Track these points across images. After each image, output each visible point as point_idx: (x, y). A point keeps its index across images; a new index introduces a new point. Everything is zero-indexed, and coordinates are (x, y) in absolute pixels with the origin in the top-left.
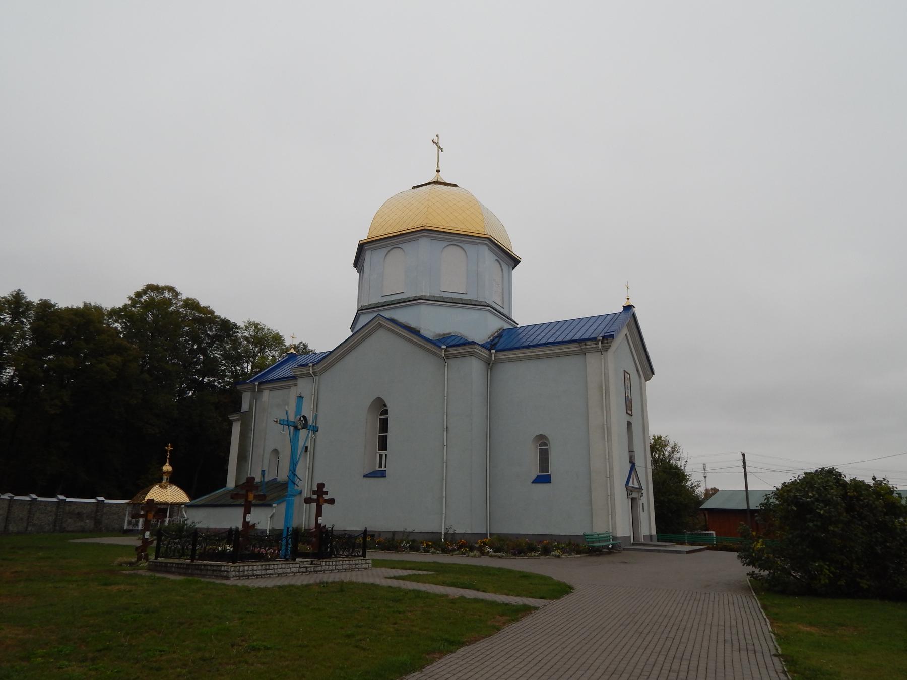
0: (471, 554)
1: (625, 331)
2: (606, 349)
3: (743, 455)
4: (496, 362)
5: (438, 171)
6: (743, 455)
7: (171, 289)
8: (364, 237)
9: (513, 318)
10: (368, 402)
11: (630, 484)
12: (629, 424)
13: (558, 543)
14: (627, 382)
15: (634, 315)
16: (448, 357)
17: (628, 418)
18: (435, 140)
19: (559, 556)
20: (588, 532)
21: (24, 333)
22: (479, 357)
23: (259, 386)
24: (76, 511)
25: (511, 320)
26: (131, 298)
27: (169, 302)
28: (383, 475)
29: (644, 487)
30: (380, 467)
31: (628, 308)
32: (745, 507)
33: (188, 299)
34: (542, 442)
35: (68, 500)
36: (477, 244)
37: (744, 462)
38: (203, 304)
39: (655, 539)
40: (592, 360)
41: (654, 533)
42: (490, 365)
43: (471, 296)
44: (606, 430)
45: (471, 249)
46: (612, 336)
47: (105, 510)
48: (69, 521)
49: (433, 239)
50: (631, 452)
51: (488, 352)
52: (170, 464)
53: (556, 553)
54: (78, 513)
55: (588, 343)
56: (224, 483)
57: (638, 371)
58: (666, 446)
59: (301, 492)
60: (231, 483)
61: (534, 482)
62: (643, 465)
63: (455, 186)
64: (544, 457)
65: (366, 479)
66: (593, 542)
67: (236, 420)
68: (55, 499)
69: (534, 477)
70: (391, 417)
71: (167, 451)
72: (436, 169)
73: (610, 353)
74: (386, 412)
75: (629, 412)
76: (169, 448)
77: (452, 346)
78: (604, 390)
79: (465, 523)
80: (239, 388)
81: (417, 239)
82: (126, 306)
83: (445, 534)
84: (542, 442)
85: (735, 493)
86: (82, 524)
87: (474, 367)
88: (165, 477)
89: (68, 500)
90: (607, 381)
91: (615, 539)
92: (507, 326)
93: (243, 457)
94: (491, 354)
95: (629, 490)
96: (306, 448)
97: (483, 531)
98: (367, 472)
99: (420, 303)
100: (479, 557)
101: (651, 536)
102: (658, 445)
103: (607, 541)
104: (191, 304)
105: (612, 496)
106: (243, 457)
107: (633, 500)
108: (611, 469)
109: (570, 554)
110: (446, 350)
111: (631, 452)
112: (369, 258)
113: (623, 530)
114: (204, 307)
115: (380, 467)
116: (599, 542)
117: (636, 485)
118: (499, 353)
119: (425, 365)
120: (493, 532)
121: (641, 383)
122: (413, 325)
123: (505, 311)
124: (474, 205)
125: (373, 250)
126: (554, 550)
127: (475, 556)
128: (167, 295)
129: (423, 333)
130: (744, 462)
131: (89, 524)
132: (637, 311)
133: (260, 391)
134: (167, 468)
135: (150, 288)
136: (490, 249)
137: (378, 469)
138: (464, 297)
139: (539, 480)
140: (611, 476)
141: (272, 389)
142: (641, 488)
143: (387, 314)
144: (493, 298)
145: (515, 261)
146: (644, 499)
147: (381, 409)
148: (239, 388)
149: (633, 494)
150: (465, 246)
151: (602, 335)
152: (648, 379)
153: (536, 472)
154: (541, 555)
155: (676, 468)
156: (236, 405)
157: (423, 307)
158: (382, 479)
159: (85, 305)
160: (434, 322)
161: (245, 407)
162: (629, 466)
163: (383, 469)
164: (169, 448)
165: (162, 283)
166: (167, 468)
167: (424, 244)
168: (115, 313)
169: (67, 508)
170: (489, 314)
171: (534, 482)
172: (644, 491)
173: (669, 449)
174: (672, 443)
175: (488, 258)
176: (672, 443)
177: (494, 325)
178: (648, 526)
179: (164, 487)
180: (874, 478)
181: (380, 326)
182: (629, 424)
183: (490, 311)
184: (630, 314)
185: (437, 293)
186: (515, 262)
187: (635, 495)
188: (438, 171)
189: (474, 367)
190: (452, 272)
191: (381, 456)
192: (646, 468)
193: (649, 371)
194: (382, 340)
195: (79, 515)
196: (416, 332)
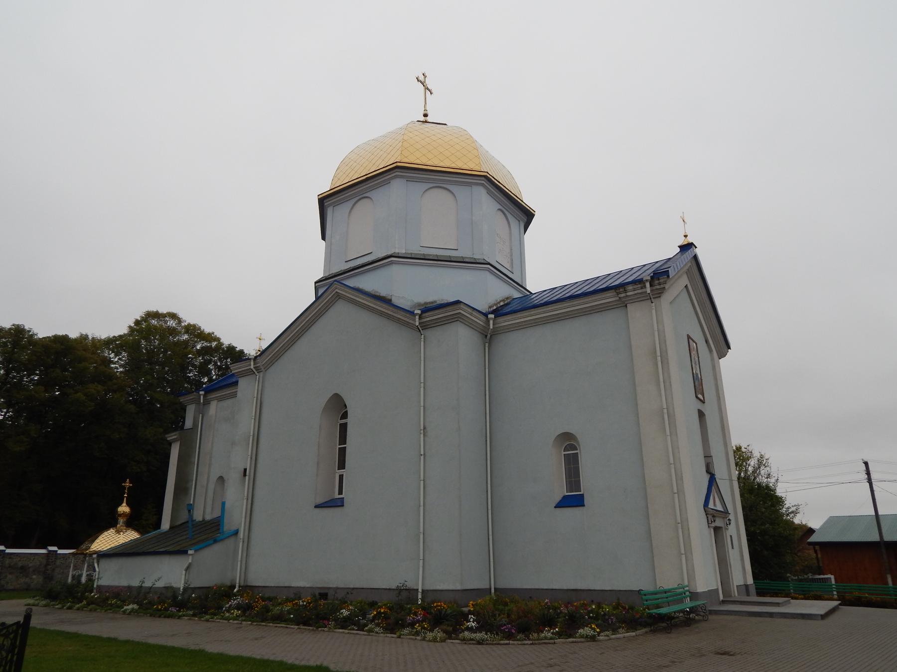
0: (430, 635)
1: (684, 281)
2: (658, 293)
3: (866, 464)
4: (496, 333)
6: (866, 464)
7: (173, 316)
8: (325, 187)
11: (711, 505)
12: (701, 414)
13: (599, 606)
14: (694, 353)
15: (695, 257)
16: (425, 326)
17: (699, 406)
18: (422, 78)
19: (593, 638)
20: (645, 585)
22: (470, 325)
23: (205, 396)
24: (20, 564)
26: (130, 327)
27: (173, 331)
28: (338, 503)
29: (730, 510)
31: (686, 247)
32: (875, 538)
33: (189, 325)
34: (568, 443)
35: (8, 551)
36: (470, 184)
37: (868, 473)
38: (207, 329)
39: (753, 590)
40: (637, 313)
41: (750, 580)
42: (488, 337)
44: (666, 417)
45: (462, 192)
46: (667, 273)
47: (58, 562)
48: (10, 576)
50: (708, 457)
51: (483, 318)
52: (128, 504)
53: (586, 631)
54: (22, 568)
55: (630, 287)
56: (158, 525)
57: (707, 341)
58: (748, 458)
59: (236, 533)
60: (165, 525)
61: (558, 506)
62: (726, 476)
64: (572, 466)
65: (318, 510)
66: (658, 607)
67: (175, 440)
68: (43, 551)
69: (558, 498)
70: (350, 420)
71: (124, 488)
72: (422, 112)
73: (667, 297)
74: (345, 415)
75: (700, 396)
76: (127, 484)
77: (435, 315)
78: (659, 356)
79: (447, 571)
80: (182, 399)
81: (388, 182)
82: (125, 335)
83: (423, 591)
84: (568, 443)
85: (852, 520)
86: (27, 580)
87: (461, 340)
88: (121, 521)
89: (8, 551)
90: (663, 342)
91: (694, 596)
92: (517, 295)
93: (182, 489)
94: (488, 320)
95: (711, 515)
98: (320, 501)
99: (392, 263)
100: (443, 641)
101: (747, 586)
102: (741, 457)
103: (681, 601)
104: (194, 331)
105: (684, 524)
106: (182, 489)
107: (716, 529)
108: (680, 479)
109: (615, 631)
110: (420, 317)
111: (708, 457)
113: (705, 580)
114: (209, 334)
115: (340, 492)
119: (395, 340)
121: (712, 359)
122: (383, 293)
125: (335, 205)
126: (583, 626)
127: (434, 640)
128: (172, 323)
129: (395, 301)
130: (868, 473)
131: (37, 579)
132: (699, 252)
133: (207, 403)
134: (124, 508)
135: (150, 315)
136: (489, 193)
137: (337, 496)
138: (453, 254)
140: (680, 492)
141: (220, 399)
142: (726, 512)
144: (499, 258)
145: (527, 216)
146: (731, 530)
147: (338, 407)
148: (182, 399)
149: (715, 519)
152: (722, 355)
153: (561, 490)
154: (560, 635)
155: (767, 487)
156: (177, 423)
157: (395, 268)
160: (410, 287)
161: (189, 424)
162: (706, 478)
164: (127, 484)
165: (163, 310)
166: (124, 508)
168: (109, 343)
169: (7, 561)
171: (558, 506)
172: (731, 517)
173: (753, 462)
174: (756, 454)
175: (486, 205)
176: (756, 454)
178: (742, 572)
179: (118, 532)
181: (338, 297)
182: (701, 414)
184: (689, 254)
185: (415, 250)
187: (719, 523)
189: (461, 340)
190: (437, 221)
191: (341, 477)
192: (731, 480)
193: (723, 344)
194: (342, 314)
195: (24, 569)
196: (386, 301)
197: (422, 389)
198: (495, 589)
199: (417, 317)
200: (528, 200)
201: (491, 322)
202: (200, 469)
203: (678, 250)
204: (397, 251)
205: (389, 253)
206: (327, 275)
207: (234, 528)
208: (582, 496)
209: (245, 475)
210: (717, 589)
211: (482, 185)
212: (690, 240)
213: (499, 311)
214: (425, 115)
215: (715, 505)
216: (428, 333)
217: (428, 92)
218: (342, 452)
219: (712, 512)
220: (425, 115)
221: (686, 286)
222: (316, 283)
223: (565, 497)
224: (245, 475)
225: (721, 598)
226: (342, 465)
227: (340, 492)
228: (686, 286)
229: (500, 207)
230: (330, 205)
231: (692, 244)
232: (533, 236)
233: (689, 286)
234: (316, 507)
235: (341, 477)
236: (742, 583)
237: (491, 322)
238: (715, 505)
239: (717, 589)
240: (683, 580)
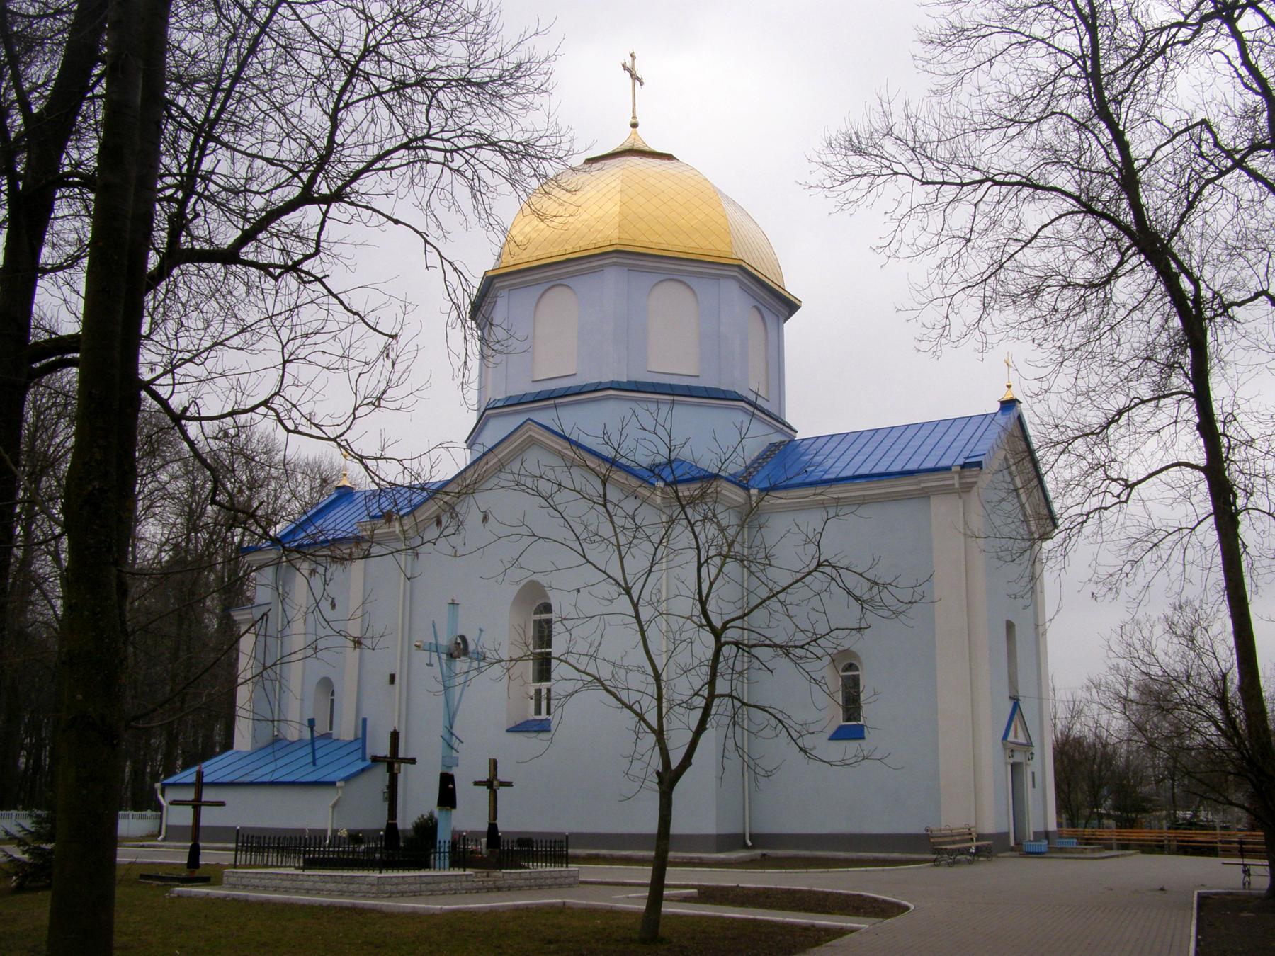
2: (967, 488)
5: (634, 126)
9: (788, 420)
10: (460, 763)
11: (1011, 737)
15: (1020, 419)
18: (629, 65)
21: (151, 315)
25: (784, 423)
28: (543, 727)
29: (1035, 742)
30: (538, 712)
31: (1009, 405)
43: (708, 381)
49: (632, 269)
56: (228, 745)
63: (669, 157)
69: (831, 730)
72: (630, 120)
81: (599, 269)
95: (1011, 749)
97: (738, 830)
112: (500, 311)
115: (538, 712)
116: (954, 842)
123: (773, 410)
124: (715, 196)
125: (511, 288)
136: (743, 287)
138: (693, 383)
139: (841, 734)
142: (1029, 744)
143: (546, 417)
144: (750, 382)
150: (693, 282)
151: (961, 461)
162: (1009, 706)
163: (544, 716)
167: (612, 281)
172: (1036, 750)
175: (736, 304)
181: (532, 442)
183: (743, 409)
184: (1012, 415)
186: (790, 306)
187: (1018, 757)
188: (634, 126)
190: (673, 337)
200: (792, 287)
203: (998, 406)
208: (862, 726)
210: (1007, 834)
211: (733, 277)
215: (1016, 736)
216: (351, 108)
217: (637, 83)
219: (1012, 746)
223: (840, 728)
225: (1012, 843)
230: (505, 292)
232: (792, 327)
236: (1041, 829)
238: (1016, 736)
239: (1007, 834)
240: (1046, 824)
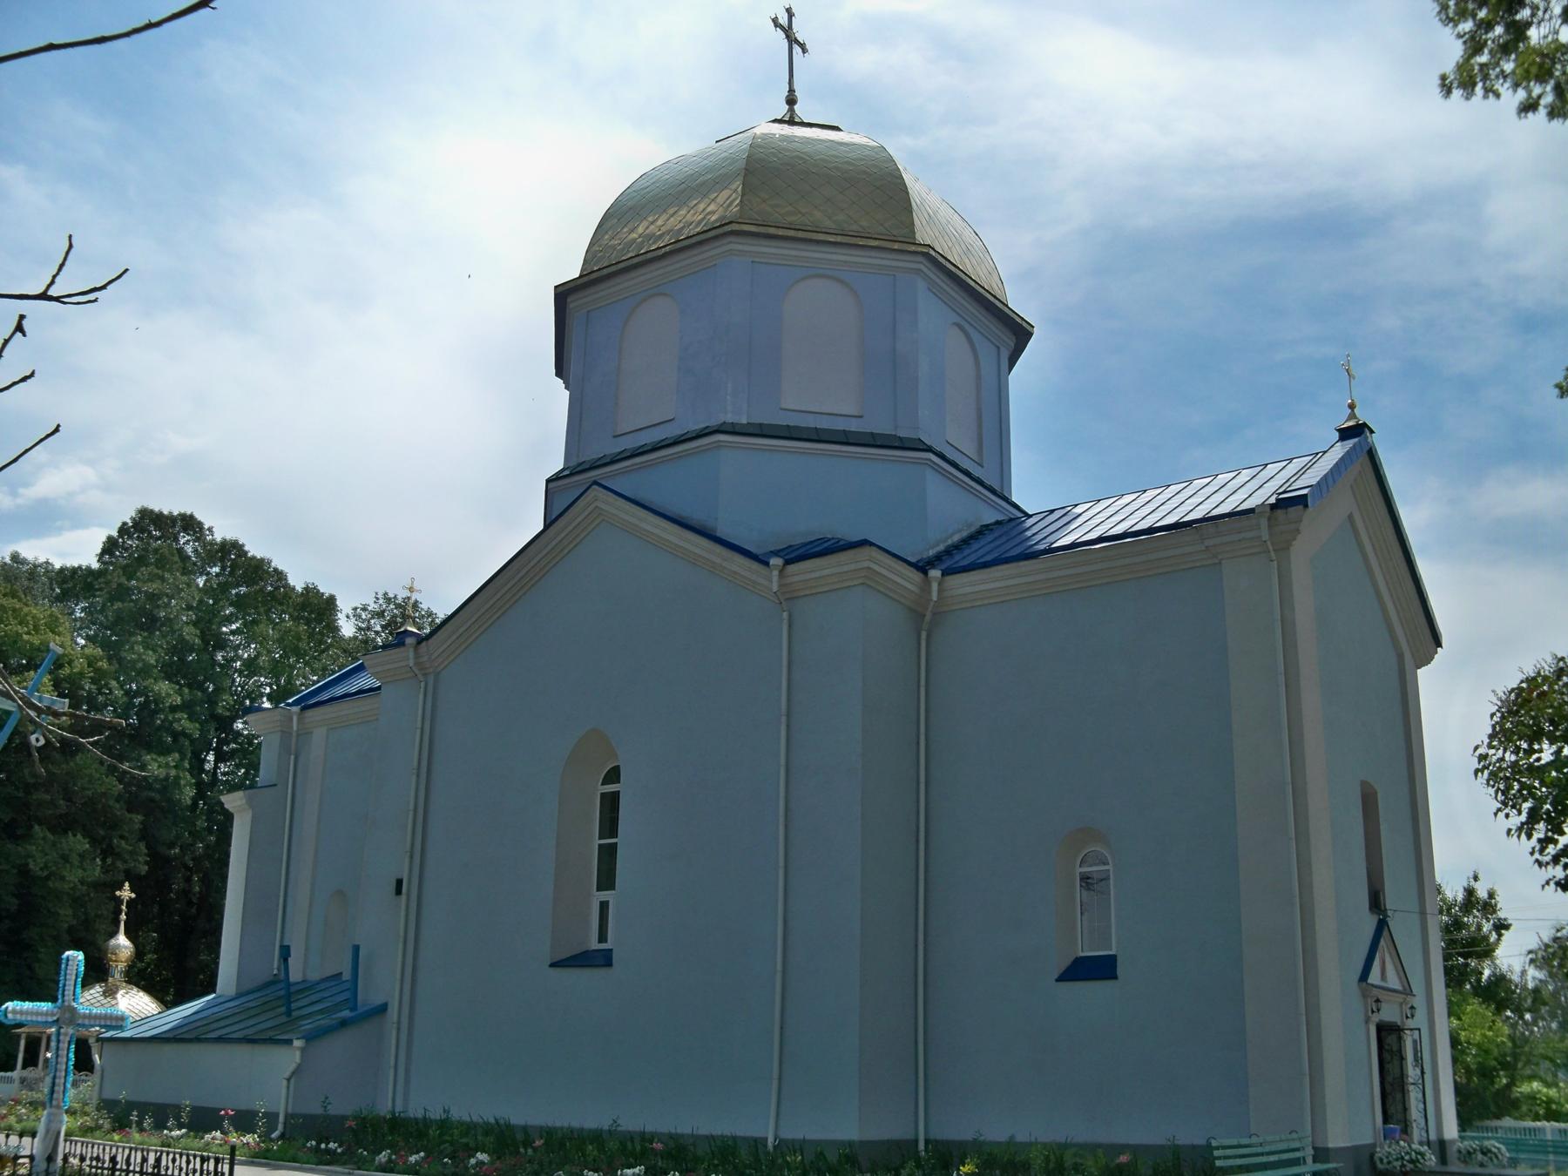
11: (1375, 977)
15: (1371, 454)
18: (783, 20)
28: (604, 959)
32: (320, 1111)
59: (383, 1009)
61: (1064, 977)
65: (558, 970)
71: (119, 901)
76: (126, 893)
96: (399, 883)
115: (602, 938)
117: (1393, 981)
118: (792, 568)
120: (937, 1134)
137: (594, 945)
138: (853, 426)
142: (1408, 991)
158: (1110, 983)
159: (307, 589)
170: (931, 478)
171: (1064, 977)
172: (1419, 1001)
177: (949, 511)
180: (1491, 895)
187: (1389, 1014)
191: (604, 906)
197: (783, 727)
198: (927, 1142)
199: (776, 573)
200: (1019, 302)
201: (935, 586)
202: (292, 875)
203: (1337, 434)
204: (730, 418)
205: (713, 422)
206: (573, 463)
207: (378, 1000)
209: (399, 891)
212: (1363, 416)
213: (952, 559)
214: (791, 101)
217: (797, 49)
218: (608, 855)
220: (791, 101)
221: (1350, 517)
222: (548, 481)
224: (399, 891)
226: (607, 879)
227: (602, 938)
228: (1350, 517)
229: (958, 320)
231: (1365, 425)
233: (1357, 517)
234: (553, 965)
235: (604, 906)
237: (935, 586)
